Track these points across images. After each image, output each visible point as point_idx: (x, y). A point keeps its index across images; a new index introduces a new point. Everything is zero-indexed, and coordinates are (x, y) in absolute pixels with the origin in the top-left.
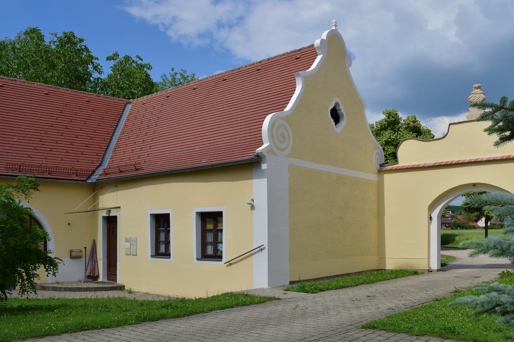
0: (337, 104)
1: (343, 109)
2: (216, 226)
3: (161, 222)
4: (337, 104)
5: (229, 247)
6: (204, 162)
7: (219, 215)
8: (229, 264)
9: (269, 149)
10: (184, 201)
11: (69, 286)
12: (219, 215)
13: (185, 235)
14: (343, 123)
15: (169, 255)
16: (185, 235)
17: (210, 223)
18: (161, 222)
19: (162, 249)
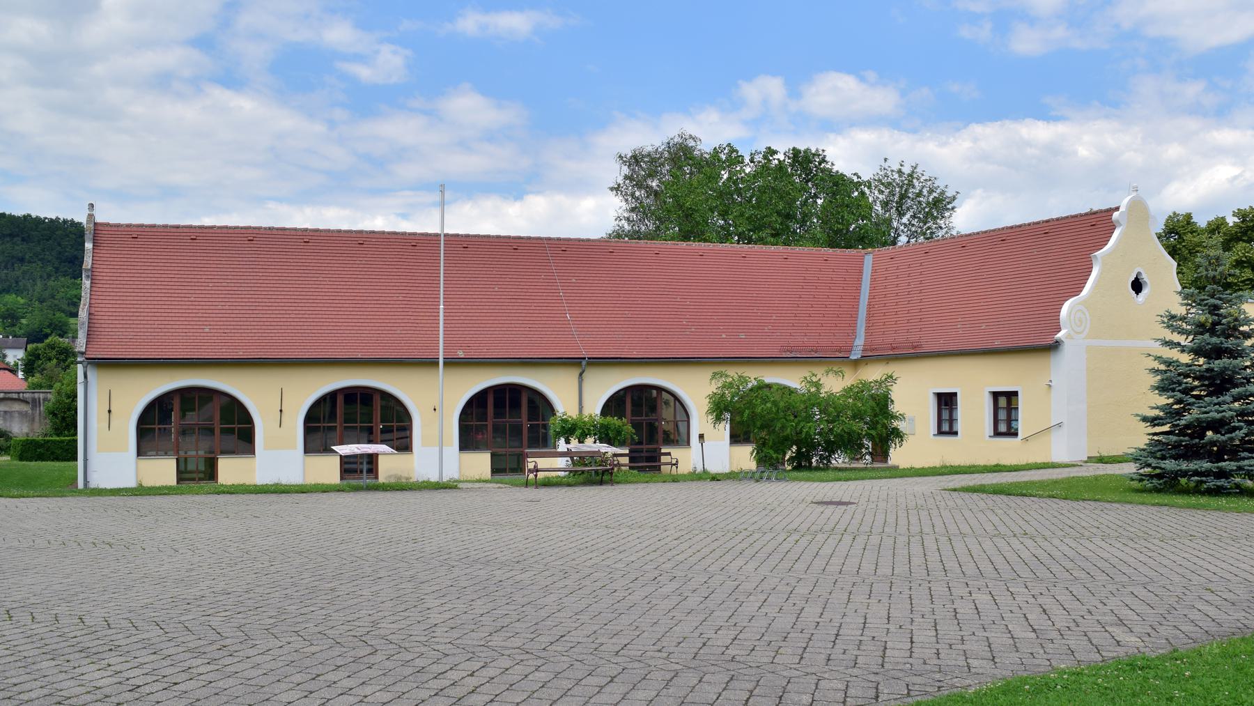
0: (1139, 273)
1: (1145, 277)
2: (722, 165)
3: (946, 401)
4: (1139, 273)
5: (1024, 424)
6: (997, 344)
7: (1015, 394)
8: (1026, 439)
9: (1068, 336)
10: (975, 383)
11: (840, 474)
12: (1015, 394)
13: (975, 413)
14: (1145, 292)
15: (956, 433)
16: (975, 413)
17: (1005, 403)
18: (946, 401)
19: (946, 427)
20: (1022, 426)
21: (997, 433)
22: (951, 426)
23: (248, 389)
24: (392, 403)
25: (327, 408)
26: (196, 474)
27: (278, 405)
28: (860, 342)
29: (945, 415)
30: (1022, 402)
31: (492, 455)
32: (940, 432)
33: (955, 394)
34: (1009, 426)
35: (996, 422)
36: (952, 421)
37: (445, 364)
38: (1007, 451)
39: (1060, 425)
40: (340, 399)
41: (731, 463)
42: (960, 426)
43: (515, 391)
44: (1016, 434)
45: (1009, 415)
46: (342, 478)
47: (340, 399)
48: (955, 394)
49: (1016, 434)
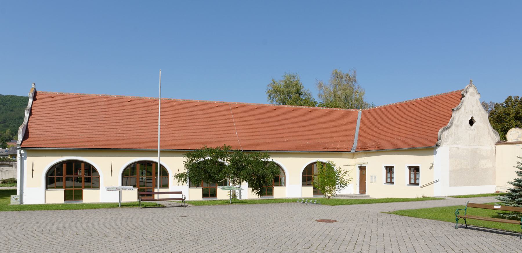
0: (472, 117)
1: (475, 118)
3: (390, 169)
4: (472, 117)
8: (422, 187)
10: (402, 162)
16: (402, 175)
18: (390, 169)
19: (413, 181)
20: (421, 182)
21: (411, 184)
22: (391, 180)
23: (95, 161)
24: (57, 166)
25: (58, 169)
26: (146, 193)
27: (109, 168)
28: (355, 145)
29: (389, 175)
30: (395, 170)
31: (65, 191)
32: (387, 183)
33: (393, 167)
34: (391, 180)
35: (410, 178)
36: (392, 178)
37: (161, 151)
38: (414, 192)
39: (437, 181)
40: (65, 166)
41: (45, 202)
42: (395, 180)
43: (150, 164)
44: (418, 184)
45: (391, 176)
46: (65, 200)
47: (65, 166)
48: (393, 167)
49: (418, 184)
